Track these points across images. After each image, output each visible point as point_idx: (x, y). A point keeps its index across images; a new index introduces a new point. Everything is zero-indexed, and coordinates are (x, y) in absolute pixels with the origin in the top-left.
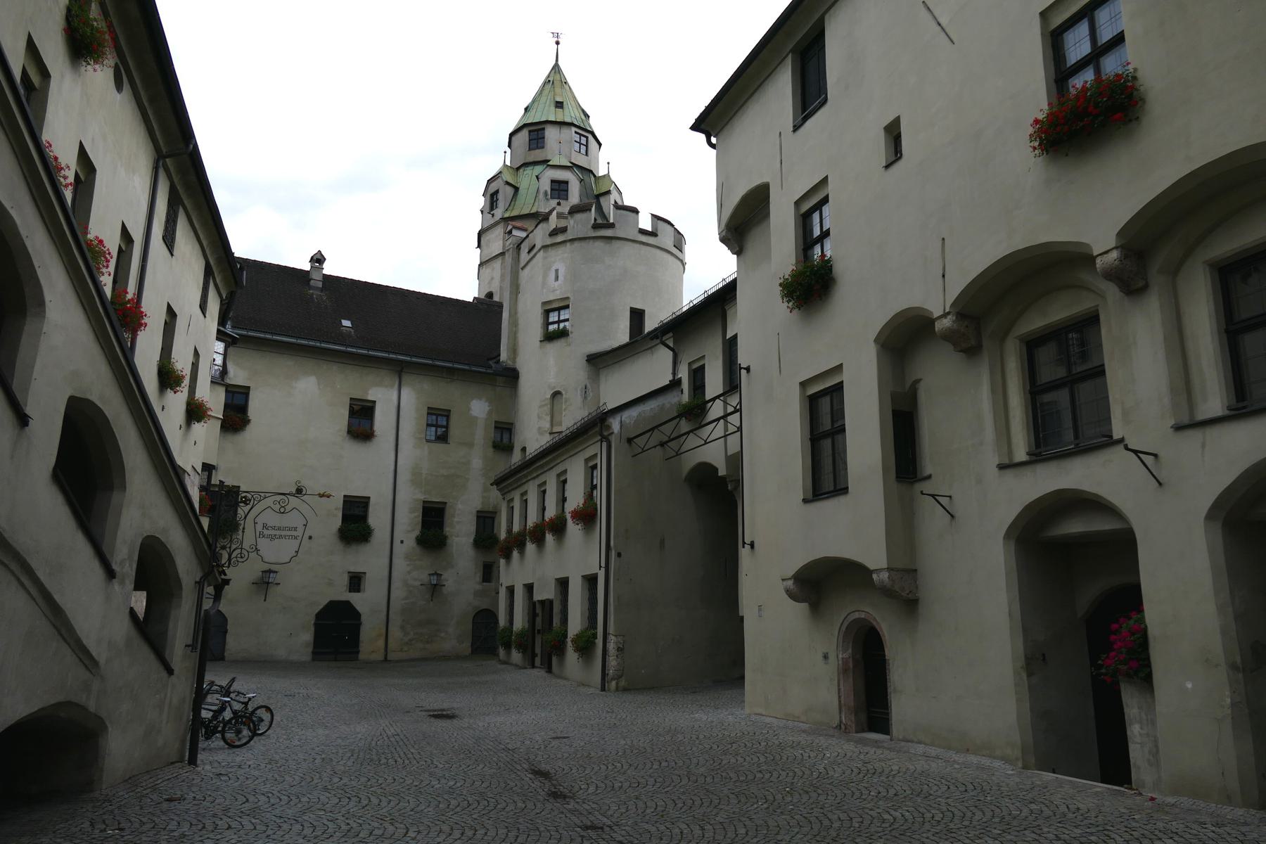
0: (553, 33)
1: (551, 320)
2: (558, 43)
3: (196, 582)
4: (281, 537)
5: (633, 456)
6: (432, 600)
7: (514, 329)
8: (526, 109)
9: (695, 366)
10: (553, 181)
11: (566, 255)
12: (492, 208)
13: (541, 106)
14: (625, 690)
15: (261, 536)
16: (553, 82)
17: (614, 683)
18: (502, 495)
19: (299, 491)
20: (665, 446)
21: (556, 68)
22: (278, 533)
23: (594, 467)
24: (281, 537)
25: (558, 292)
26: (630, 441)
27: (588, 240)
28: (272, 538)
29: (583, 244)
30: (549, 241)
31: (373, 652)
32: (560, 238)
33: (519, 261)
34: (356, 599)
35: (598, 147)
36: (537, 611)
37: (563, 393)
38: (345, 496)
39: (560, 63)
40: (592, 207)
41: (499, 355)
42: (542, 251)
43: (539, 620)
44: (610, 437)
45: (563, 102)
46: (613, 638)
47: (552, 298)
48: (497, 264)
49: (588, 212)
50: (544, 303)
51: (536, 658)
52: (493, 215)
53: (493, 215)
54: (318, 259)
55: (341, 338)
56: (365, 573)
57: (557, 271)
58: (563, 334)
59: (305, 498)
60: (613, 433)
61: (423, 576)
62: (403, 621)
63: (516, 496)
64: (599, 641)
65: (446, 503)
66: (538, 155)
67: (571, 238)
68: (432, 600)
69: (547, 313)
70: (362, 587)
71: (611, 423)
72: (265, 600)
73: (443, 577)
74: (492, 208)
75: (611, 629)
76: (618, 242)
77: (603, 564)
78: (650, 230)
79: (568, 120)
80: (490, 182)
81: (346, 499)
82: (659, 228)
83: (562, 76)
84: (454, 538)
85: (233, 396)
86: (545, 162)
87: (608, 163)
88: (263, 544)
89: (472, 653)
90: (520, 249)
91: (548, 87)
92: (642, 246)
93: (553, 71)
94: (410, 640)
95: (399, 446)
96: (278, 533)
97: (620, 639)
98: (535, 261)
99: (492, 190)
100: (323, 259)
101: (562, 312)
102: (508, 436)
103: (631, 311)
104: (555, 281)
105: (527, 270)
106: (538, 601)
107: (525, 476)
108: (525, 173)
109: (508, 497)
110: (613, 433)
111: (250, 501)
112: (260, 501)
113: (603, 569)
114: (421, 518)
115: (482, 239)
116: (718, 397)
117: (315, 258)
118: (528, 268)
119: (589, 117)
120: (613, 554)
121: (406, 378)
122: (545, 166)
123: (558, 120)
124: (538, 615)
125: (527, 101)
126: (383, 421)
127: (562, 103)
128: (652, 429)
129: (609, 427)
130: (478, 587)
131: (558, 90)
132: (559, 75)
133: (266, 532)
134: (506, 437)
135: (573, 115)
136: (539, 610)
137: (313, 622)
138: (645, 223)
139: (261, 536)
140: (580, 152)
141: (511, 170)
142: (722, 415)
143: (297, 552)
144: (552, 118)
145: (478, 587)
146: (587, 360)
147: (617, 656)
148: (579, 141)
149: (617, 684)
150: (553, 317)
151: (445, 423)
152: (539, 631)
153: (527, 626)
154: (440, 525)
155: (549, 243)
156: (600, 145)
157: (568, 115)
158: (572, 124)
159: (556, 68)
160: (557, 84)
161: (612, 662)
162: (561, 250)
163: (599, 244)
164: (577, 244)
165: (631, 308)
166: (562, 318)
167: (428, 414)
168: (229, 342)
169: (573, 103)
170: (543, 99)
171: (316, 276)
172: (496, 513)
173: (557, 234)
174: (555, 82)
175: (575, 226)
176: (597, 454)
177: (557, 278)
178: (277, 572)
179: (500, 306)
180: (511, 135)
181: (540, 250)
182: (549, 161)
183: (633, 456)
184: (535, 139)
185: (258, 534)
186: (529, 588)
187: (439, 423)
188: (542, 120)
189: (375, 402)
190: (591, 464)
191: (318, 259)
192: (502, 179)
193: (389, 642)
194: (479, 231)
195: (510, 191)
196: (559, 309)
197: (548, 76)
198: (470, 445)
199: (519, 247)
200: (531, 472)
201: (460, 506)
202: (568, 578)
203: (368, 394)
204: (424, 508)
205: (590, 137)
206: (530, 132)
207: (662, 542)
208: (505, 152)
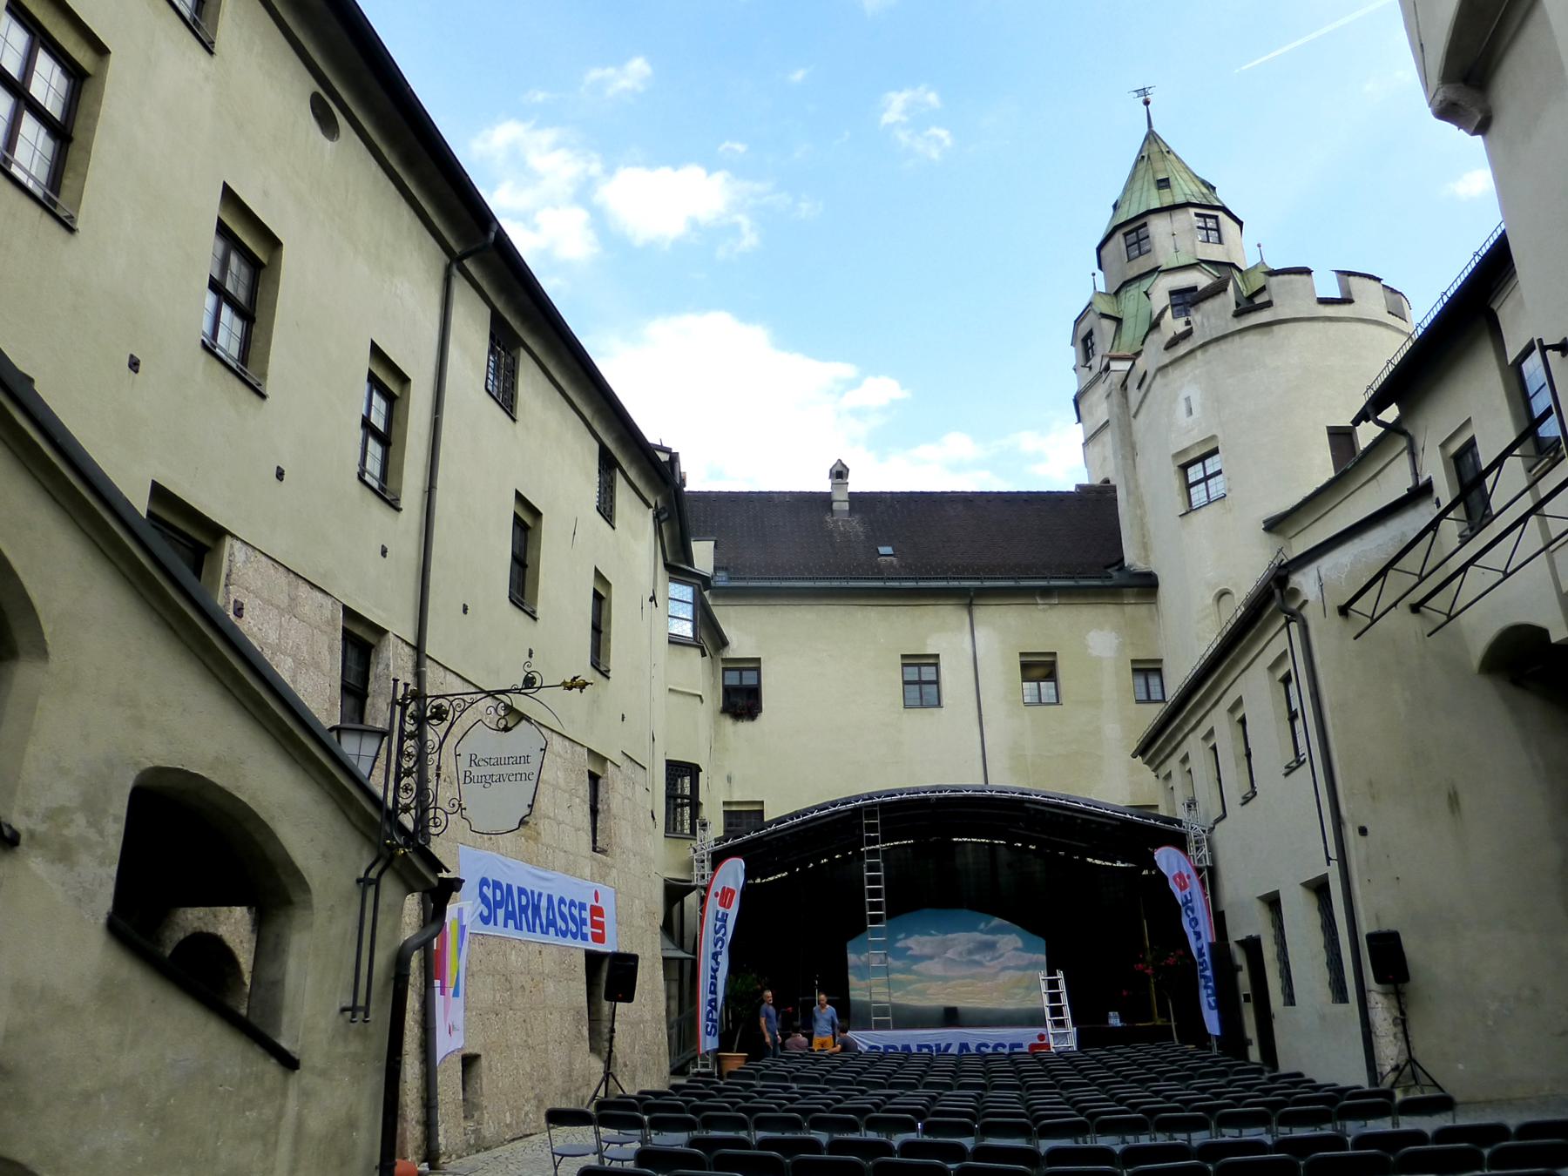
1: (1191, 480)
2: (1147, 103)
3: (359, 881)
4: (501, 778)
5: (1355, 638)
7: (1138, 512)
8: (1115, 207)
9: (1455, 447)
10: (1172, 293)
11: (1197, 372)
12: (1087, 359)
15: (468, 780)
18: (1154, 770)
19: (529, 682)
20: (1422, 609)
21: (1151, 137)
22: (496, 770)
23: (1286, 680)
24: (501, 778)
25: (1195, 432)
26: (1344, 611)
27: (1230, 339)
28: (487, 780)
29: (1224, 345)
30: (1167, 358)
32: (1183, 349)
33: (1128, 407)
35: (1238, 227)
37: (1234, 591)
39: (1155, 128)
40: (1227, 285)
41: (1123, 559)
42: (1158, 377)
45: (1168, 179)
47: (1186, 444)
48: (1107, 437)
49: (1222, 295)
50: (1176, 456)
51: (1250, 1048)
52: (1090, 368)
53: (1090, 368)
54: (840, 473)
55: (878, 573)
57: (1188, 399)
59: (539, 694)
60: (1306, 602)
67: (1201, 342)
69: (1184, 468)
71: (1299, 582)
74: (1087, 359)
76: (1284, 326)
77: (1333, 854)
78: (1339, 297)
79: (1180, 199)
80: (1078, 322)
83: (1161, 144)
85: (741, 675)
86: (1156, 271)
87: (1259, 246)
88: (472, 794)
90: (1126, 389)
91: (1142, 166)
92: (1328, 324)
93: (1147, 142)
96: (496, 770)
98: (1150, 395)
99: (1083, 332)
100: (845, 471)
101: (1208, 462)
103: (1330, 434)
104: (1188, 416)
105: (1141, 417)
107: (1179, 728)
108: (1128, 295)
109: (1163, 771)
111: (447, 712)
112: (463, 711)
113: (1335, 864)
115: (1081, 407)
116: (1508, 452)
117: (834, 471)
119: (1214, 188)
120: (1350, 832)
122: (1156, 274)
123: (1165, 205)
125: (1116, 194)
126: (953, 678)
128: (1383, 573)
129: (1295, 593)
131: (1158, 165)
132: (1155, 146)
133: (476, 771)
135: (1188, 192)
139: (468, 780)
140: (1208, 241)
141: (1107, 298)
142: (1531, 505)
143: (531, 806)
144: (1155, 205)
148: (1209, 232)
150: (1195, 473)
155: (1167, 361)
156: (1240, 223)
157: (1183, 190)
158: (1189, 205)
159: (1151, 137)
160: (1156, 157)
162: (1189, 366)
163: (1251, 338)
164: (1213, 349)
166: (1209, 472)
168: (699, 585)
169: (1185, 176)
171: (840, 497)
174: (1151, 156)
175: (1205, 321)
176: (1286, 650)
177: (1190, 412)
179: (1114, 489)
180: (1099, 249)
181: (1154, 377)
182: (1159, 267)
183: (1355, 638)
184: (1133, 244)
185: (462, 777)
188: (1141, 212)
190: (1281, 673)
191: (840, 473)
192: (1095, 312)
194: (1075, 397)
195: (1108, 325)
196: (1202, 459)
197: (1141, 152)
199: (1124, 385)
200: (1185, 720)
202: (1278, 891)
205: (1221, 215)
206: (1125, 235)
207: (1454, 800)
208: (1094, 274)
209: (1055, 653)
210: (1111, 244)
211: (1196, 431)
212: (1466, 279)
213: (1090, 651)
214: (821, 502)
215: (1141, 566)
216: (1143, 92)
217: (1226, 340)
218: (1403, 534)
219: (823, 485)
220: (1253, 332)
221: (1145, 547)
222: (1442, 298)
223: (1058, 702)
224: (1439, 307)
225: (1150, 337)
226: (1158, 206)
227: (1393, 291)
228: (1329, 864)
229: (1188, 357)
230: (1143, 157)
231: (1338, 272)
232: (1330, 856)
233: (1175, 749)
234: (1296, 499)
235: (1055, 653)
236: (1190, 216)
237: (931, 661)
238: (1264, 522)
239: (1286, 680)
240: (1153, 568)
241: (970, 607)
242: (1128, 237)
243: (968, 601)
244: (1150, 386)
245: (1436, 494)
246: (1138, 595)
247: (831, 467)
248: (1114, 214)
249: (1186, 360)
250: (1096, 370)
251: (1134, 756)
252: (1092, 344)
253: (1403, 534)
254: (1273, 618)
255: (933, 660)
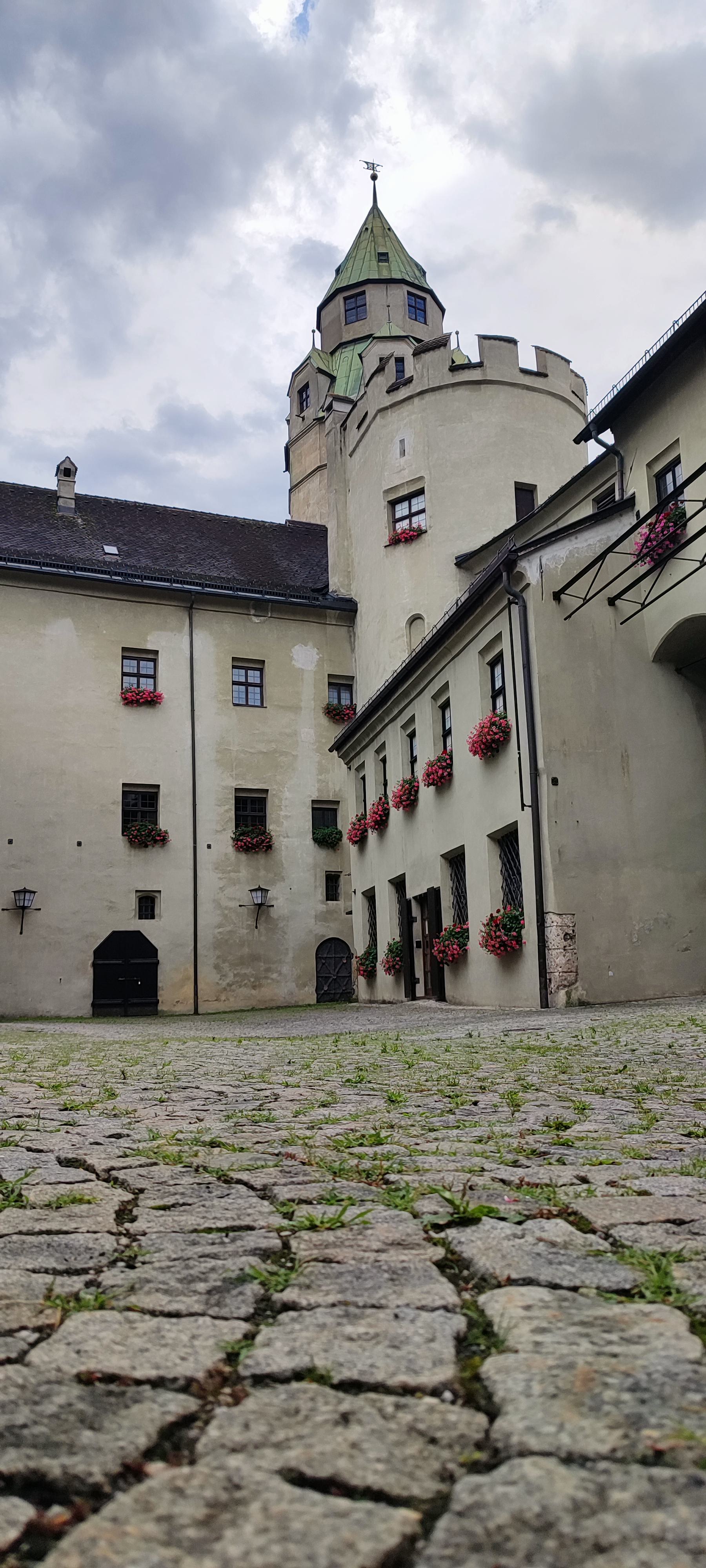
0: (367, 163)
1: (398, 515)
2: (374, 177)
5: (565, 619)
6: (256, 927)
8: (338, 271)
11: (413, 417)
12: (302, 410)
13: (358, 263)
14: (583, 1004)
16: (372, 231)
17: (562, 993)
21: (375, 211)
26: (557, 596)
27: (444, 391)
29: (437, 395)
30: (388, 400)
31: (178, 1002)
32: (403, 393)
34: (146, 927)
36: (414, 915)
37: (425, 616)
38: (124, 785)
41: (327, 586)
42: (378, 417)
43: (417, 927)
44: (524, 595)
46: (555, 918)
49: (442, 348)
51: (417, 986)
52: (303, 418)
53: (303, 418)
56: (159, 892)
57: (402, 442)
58: (413, 536)
60: (528, 585)
61: (241, 894)
62: (218, 957)
63: (369, 757)
64: (530, 933)
65: (267, 791)
66: (359, 329)
67: (418, 391)
68: (256, 927)
69: (393, 504)
70: (157, 912)
72: (21, 933)
73: (269, 894)
75: (550, 904)
77: (528, 801)
79: (397, 275)
80: (295, 374)
81: (126, 789)
82: (549, 364)
84: (281, 838)
89: (318, 1002)
90: (345, 429)
94: (229, 985)
95: (196, 713)
97: (567, 920)
99: (299, 385)
100: (73, 469)
101: (414, 501)
102: (348, 695)
103: (516, 489)
105: (356, 455)
106: (415, 898)
107: (381, 719)
108: (343, 356)
109: (356, 764)
110: (528, 585)
113: (529, 811)
114: (233, 812)
117: (62, 468)
118: (360, 450)
120: (544, 782)
121: (198, 616)
124: (415, 920)
127: (386, 254)
128: (602, 557)
129: (521, 576)
130: (322, 907)
132: (378, 219)
134: (345, 696)
136: (416, 911)
137: (90, 962)
138: (528, 360)
145: (322, 907)
146: (456, 564)
147: (565, 948)
149: (568, 994)
150: (402, 510)
151: (258, 681)
152: (419, 944)
153: (398, 939)
154: (262, 820)
156: (443, 311)
159: (375, 212)
161: (557, 960)
162: (406, 408)
163: (461, 392)
164: (428, 397)
165: (516, 483)
166: (414, 510)
167: (234, 667)
170: (361, 254)
172: (338, 802)
173: (397, 388)
174: (374, 229)
177: (403, 453)
178: (34, 892)
180: (320, 309)
183: (565, 619)
186: (399, 884)
187: (250, 680)
189: (157, 652)
191: (67, 471)
193: (200, 986)
195: (324, 381)
196: (408, 498)
197: (365, 223)
198: (296, 709)
199: (344, 426)
201: (287, 794)
203: (146, 641)
204: (238, 800)
205: (428, 297)
206: (345, 299)
209: (264, 661)
210: (331, 306)
211: (407, 471)
212: (637, 373)
213: (293, 662)
214: (50, 497)
215: (343, 593)
216: (371, 166)
217: (440, 391)
218: (609, 537)
219: (49, 482)
220: (464, 387)
221: (348, 575)
222: (674, 325)
223: (262, 706)
224: (610, 398)
225: (374, 379)
226: (377, 277)
227: (577, 375)
228: (523, 810)
229: (407, 403)
230: (367, 229)
231: (537, 348)
232: (525, 802)
233: (372, 740)
234: (477, 546)
235: (264, 661)
236: (400, 294)
237: (150, 656)
238: (456, 558)
239: (493, 664)
240: (353, 595)
241: (190, 610)
242: (347, 302)
243: (189, 605)
244: (369, 426)
245: (637, 508)
246: (339, 618)
247: (59, 463)
248: (336, 278)
249: (404, 404)
250: (308, 422)
251: (331, 750)
252: (308, 397)
253: (609, 537)
254: (498, 599)
255: (152, 656)
